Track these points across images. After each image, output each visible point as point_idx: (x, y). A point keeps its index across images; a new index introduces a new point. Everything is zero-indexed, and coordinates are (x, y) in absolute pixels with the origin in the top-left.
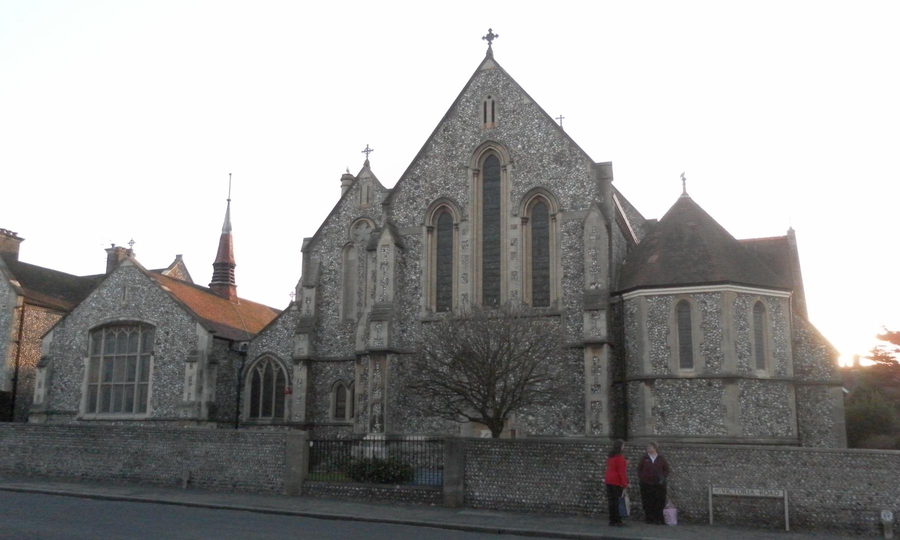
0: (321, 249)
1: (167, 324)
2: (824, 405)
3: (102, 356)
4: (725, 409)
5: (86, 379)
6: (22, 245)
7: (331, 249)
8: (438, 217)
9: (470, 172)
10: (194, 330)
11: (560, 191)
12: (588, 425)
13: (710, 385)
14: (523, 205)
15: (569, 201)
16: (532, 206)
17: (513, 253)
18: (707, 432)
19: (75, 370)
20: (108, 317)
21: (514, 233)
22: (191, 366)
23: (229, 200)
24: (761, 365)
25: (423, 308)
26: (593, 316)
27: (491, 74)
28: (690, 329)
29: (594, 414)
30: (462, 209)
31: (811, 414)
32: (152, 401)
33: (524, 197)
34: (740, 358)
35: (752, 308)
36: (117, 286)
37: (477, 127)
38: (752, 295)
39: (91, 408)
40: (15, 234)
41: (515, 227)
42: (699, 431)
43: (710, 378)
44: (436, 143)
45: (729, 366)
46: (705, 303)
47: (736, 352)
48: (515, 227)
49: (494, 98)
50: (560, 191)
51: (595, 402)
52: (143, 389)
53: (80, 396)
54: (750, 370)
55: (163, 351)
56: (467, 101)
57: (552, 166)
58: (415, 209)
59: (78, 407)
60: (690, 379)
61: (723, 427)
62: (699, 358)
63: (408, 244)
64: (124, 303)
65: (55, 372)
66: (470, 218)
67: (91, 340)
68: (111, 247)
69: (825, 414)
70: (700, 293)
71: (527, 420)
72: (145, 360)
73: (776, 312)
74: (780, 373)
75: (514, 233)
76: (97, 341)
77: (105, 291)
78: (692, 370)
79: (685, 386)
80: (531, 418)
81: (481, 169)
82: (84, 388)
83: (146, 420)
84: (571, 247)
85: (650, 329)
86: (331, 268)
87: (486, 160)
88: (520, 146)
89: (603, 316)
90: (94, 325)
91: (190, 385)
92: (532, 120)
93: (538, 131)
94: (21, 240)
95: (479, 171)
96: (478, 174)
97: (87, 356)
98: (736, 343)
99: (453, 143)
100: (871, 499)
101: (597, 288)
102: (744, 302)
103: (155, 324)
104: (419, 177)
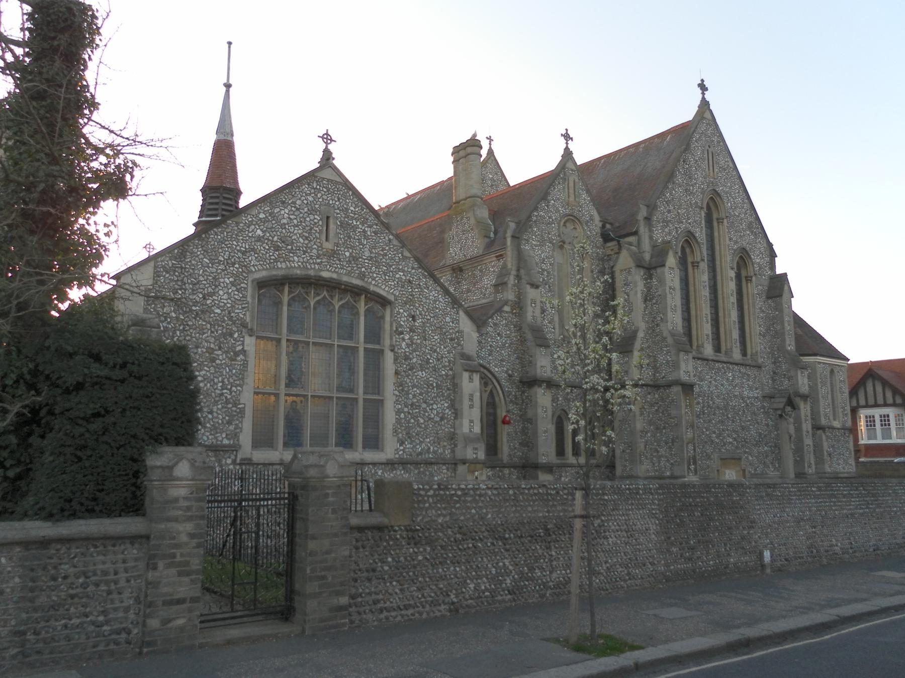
1: (410, 301)
7: (542, 243)
10: (456, 321)
19: (221, 358)
22: (471, 380)
23: (228, 86)
32: (395, 431)
48: (732, 280)
52: (375, 409)
53: (242, 412)
55: (408, 346)
59: (235, 436)
64: (328, 246)
72: (375, 358)
83: (390, 464)
84: (761, 308)
86: (544, 266)
90: (264, 274)
91: (471, 407)
103: (392, 298)
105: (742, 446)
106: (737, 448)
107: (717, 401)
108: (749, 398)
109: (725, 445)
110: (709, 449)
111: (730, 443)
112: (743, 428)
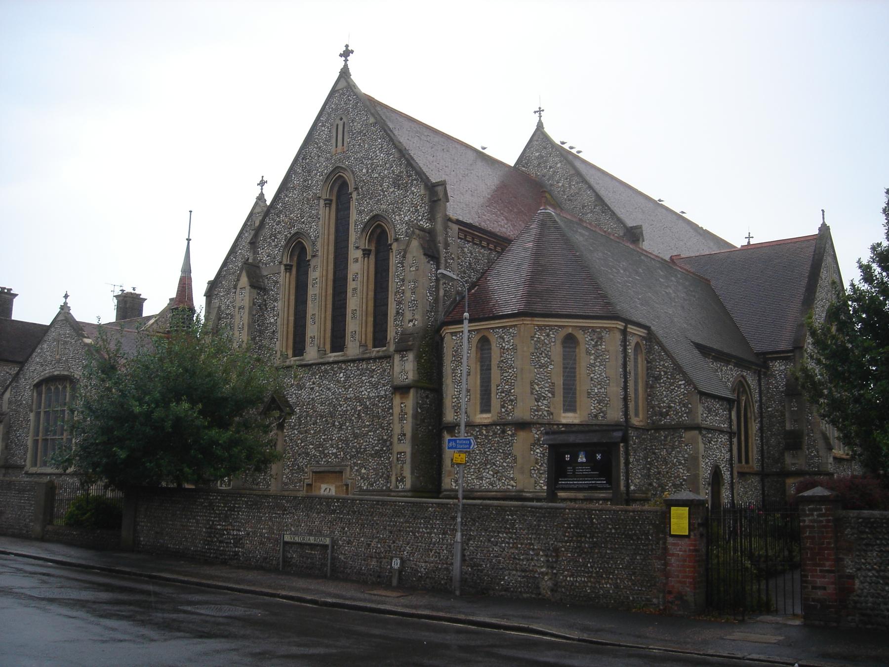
0: (220, 292)
2: (680, 452)
3: (42, 410)
4: (515, 460)
5: (31, 434)
6: (15, 301)
8: (297, 253)
9: (322, 202)
11: (397, 218)
12: (393, 479)
13: (504, 432)
14: (364, 234)
15: (404, 228)
16: (375, 236)
17: (355, 289)
18: (499, 486)
20: (48, 372)
21: (358, 268)
23: (189, 240)
24: (570, 406)
25: (279, 353)
26: (403, 357)
27: (343, 94)
28: (490, 369)
29: (399, 466)
30: (314, 244)
31: (666, 464)
33: (365, 227)
34: (537, 400)
35: (559, 343)
36: (55, 340)
37: (329, 152)
38: (560, 326)
39: (34, 464)
40: (10, 290)
41: (356, 260)
42: (491, 484)
43: (505, 425)
44: (296, 173)
45: (522, 411)
46: (504, 339)
47: (532, 393)
48: (356, 260)
49: (345, 120)
50: (397, 218)
51: (401, 453)
54: (550, 413)
56: (323, 126)
57: (391, 190)
58: (276, 246)
59: (25, 461)
60: (486, 426)
61: (513, 479)
62: (495, 403)
63: (269, 284)
64: (58, 357)
65: (11, 427)
66: (319, 254)
67: (35, 394)
68: (120, 293)
69: (680, 464)
70: (499, 328)
71: (360, 473)
73: (595, 346)
74: (596, 416)
75: (358, 268)
76: (40, 394)
77: (45, 346)
78: (576, 415)
79: (482, 434)
80: (363, 471)
81: (334, 198)
82: (30, 443)
85: (453, 370)
87: (339, 191)
88: (364, 171)
89: (411, 356)
92: (376, 140)
93: (381, 152)
94: (16, 295)
95: (331, 200)
96: (330, 204)
97: (31, 411)
98: (532, 383)
99: (309, 172)
100: (390, 547)
101: (414, 325)
102: (548, 335)
104: (281, 212)
105: (352, 457)
106: (343, 459)
107: (320, 408)
108: (369, 398)
109: (326, 456)
110: (302, 462)
111: (333, 454)
112: (356, 436)
